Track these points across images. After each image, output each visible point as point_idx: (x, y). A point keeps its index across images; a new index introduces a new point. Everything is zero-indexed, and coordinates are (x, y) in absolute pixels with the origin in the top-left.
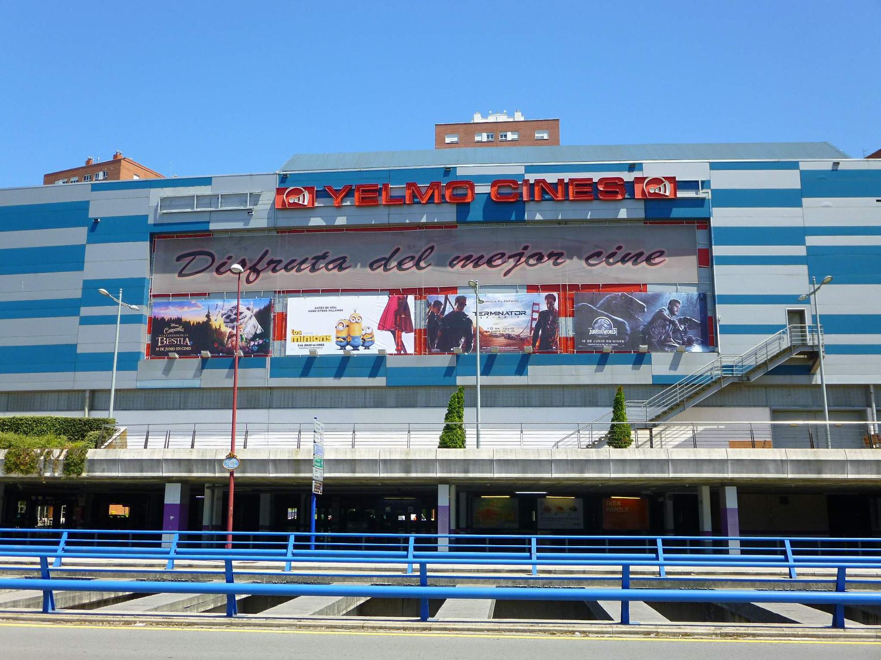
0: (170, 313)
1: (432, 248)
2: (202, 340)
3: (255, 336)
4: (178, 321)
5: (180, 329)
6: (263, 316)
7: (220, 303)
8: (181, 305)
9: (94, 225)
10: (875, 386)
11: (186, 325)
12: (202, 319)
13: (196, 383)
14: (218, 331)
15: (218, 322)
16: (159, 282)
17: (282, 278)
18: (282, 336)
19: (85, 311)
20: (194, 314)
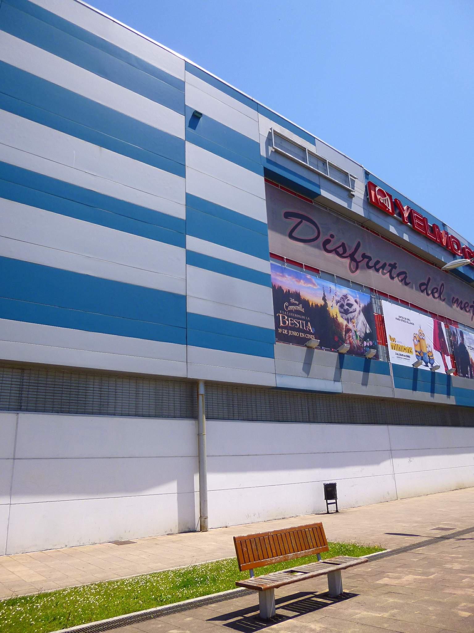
0: (288, 282)
1: (443, 285)
2: (316, 327)
3: (367, 336)
4: (297, 296)
5: (300, 308)
6: (367, 311)
7: (332, 286)
8: (298, 278)
9: (195, 118)
10: (209, 384)
11: (305, 303)
12: (320, 302)
13: (337, 387)
14: (335, 320)
15: (334, 310)
16: (277, 242)
17: (378, 279)
18: (385, 343)
19: (194, 243)
20: (312, 291)
